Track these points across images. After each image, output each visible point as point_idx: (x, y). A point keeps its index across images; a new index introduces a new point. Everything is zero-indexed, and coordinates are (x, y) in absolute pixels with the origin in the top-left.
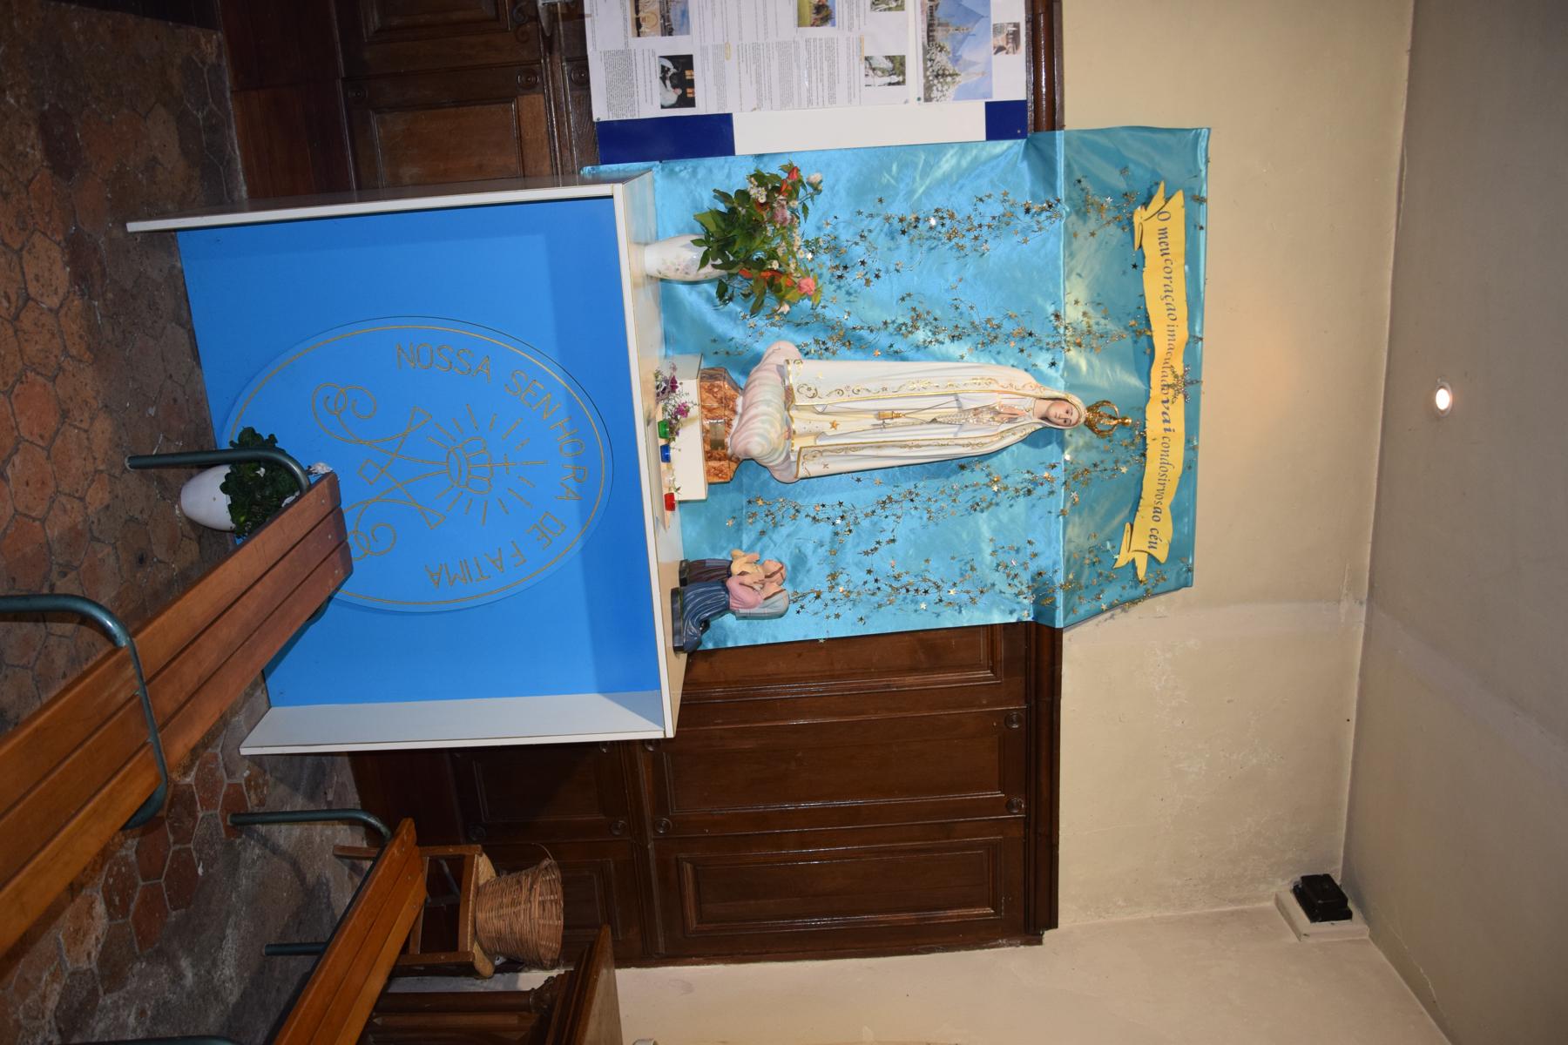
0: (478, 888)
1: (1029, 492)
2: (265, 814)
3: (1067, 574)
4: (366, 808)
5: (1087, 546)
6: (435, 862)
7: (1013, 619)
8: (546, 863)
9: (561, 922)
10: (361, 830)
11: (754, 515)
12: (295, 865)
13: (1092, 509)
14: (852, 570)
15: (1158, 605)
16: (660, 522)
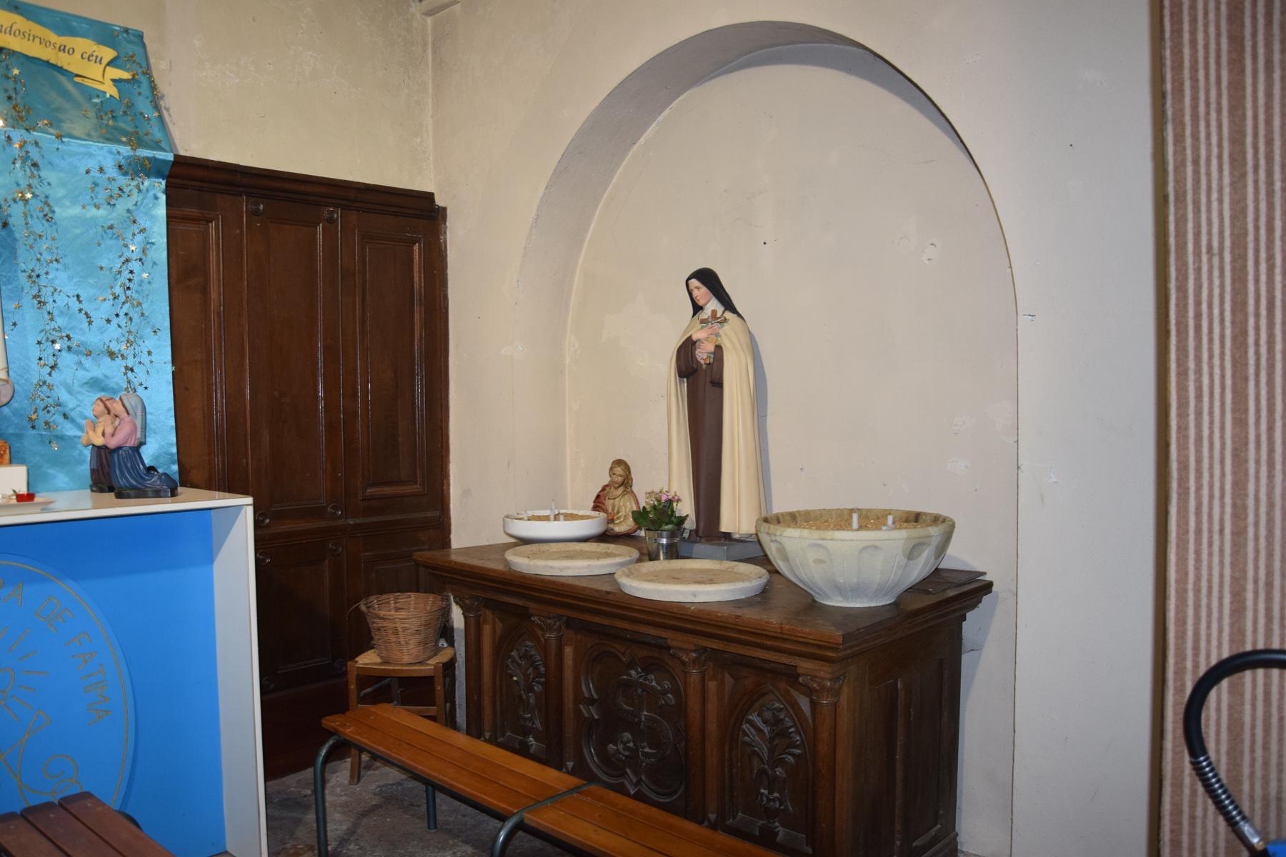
0: (386, 662)
1: (35, 165)
2: (319, 843)
3: (120, 142)
4: (311, 763)
5: (94, 121)
6: (363, 700)
7: (163, 197)
8: (363, 608)
9: (413, 594)
10: (330, 766)
11: (47, 423)
12: (364, 814)
13: (58, 109)
14: (106, 337)
15: (159, 67)
16: (45, 507)
